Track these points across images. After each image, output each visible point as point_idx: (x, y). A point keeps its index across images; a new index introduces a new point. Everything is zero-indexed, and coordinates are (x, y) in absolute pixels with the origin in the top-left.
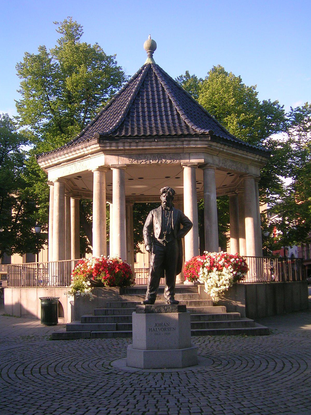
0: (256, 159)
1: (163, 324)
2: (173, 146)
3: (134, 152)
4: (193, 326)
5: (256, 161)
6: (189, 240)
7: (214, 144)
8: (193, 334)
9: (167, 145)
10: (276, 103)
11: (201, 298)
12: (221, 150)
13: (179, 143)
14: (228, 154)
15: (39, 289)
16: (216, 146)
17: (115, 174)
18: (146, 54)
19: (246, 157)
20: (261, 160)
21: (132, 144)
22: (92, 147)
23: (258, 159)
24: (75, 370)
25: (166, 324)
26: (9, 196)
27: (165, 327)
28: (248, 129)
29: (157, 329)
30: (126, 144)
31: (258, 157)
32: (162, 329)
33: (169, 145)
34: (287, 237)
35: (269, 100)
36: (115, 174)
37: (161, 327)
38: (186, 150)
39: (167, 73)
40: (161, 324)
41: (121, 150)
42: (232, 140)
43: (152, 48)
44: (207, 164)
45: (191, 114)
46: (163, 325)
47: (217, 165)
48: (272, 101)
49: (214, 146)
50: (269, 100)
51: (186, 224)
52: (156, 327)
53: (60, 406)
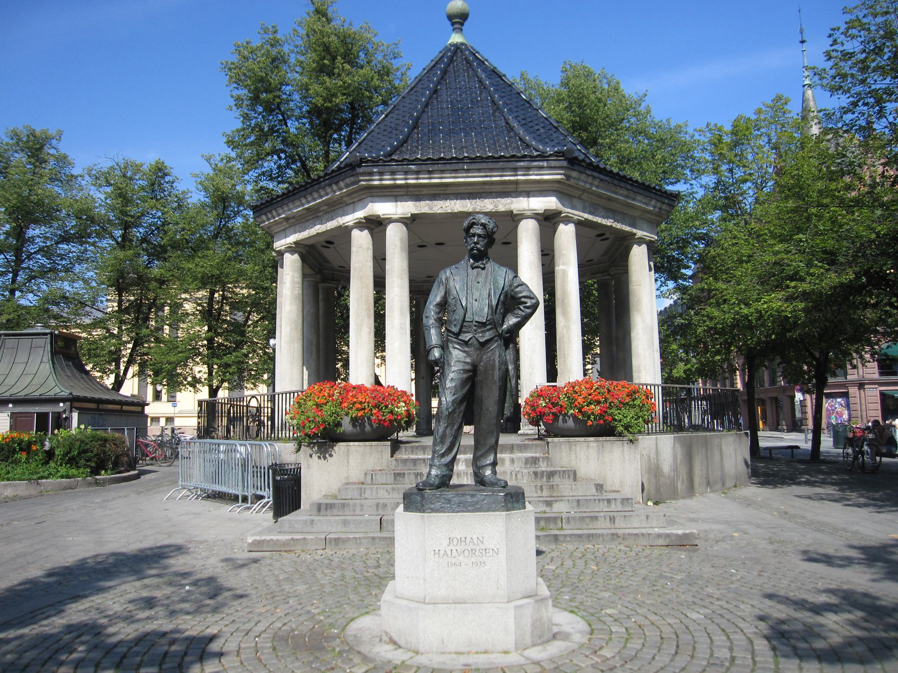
1: (468, 540)
3: (425, 191)
5: (648, 212)
6: (434, 421)
7: (574, 174)
10: (679, 129)
11: (551, 465)
12: (588, 186)
14: (599, 196)
15: (608, 445)
16: (579, 179)
20: (660, 209)
23: (654, 207)
25: (475, 540)
27: (474, 547)
29: (454, 551)
31: (653, 202)
32: (466, 553)
34: (771, 337)
35: (668, 120)
37: (464, 547)
38: (522, 186)
40: (463, 539)
46: (468, 542)
48: (673, 124)
49: (574, 178)
50: (668, 120)
51: (523, 300)
52: (452, 547)
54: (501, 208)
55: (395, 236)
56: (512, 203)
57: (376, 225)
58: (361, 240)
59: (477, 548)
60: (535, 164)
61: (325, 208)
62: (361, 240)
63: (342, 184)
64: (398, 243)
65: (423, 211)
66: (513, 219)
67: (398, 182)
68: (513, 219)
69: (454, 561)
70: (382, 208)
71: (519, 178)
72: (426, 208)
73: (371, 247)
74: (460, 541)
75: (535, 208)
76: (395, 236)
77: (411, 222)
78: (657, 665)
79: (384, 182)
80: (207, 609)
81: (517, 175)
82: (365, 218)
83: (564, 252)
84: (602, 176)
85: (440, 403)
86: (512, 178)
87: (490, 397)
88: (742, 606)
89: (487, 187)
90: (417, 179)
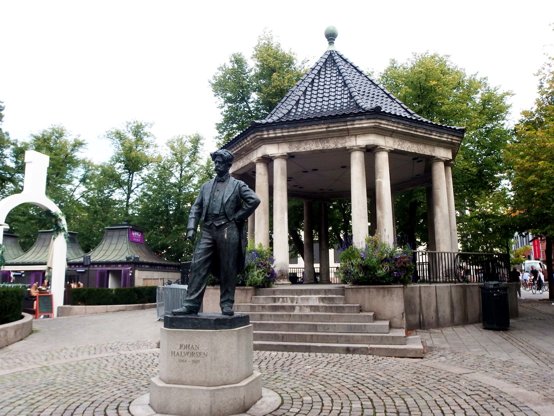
1: (191, 346)
25: (194, 346)
41: (279, 137)
43: (331, 37)
54: (340, 146)
55: (279, 166)
56: (346, 142)
57: (268, 161)
58: (260, 169)
59: (195, 352)
60: (357, 118)
61: (244, 152)
62: (260, 169)
63: (249, 139)
64: (279, 171)
65: (294, 151)
66: (347, 152)
67: (278, 135)
68: (347, 152)
69: (182, 358)
70: (271, 150)
71: (349, 127)
72: (296, 149)
73: (266, 173)
74: (186, 347)
75: (360, 144)
76: (279, 166)
77: (290, 157)
78: (335, 412)
79: (270, 136)
80: (493, 375)
81: (347, 125)
82: (262, 157)
83: (380, 170)
84: (404, 122)
85: (433, 256)
86: (344, 127)
87: (228, 262)
88: (309, 379)
89: (330, 134)
90: (289, 132)
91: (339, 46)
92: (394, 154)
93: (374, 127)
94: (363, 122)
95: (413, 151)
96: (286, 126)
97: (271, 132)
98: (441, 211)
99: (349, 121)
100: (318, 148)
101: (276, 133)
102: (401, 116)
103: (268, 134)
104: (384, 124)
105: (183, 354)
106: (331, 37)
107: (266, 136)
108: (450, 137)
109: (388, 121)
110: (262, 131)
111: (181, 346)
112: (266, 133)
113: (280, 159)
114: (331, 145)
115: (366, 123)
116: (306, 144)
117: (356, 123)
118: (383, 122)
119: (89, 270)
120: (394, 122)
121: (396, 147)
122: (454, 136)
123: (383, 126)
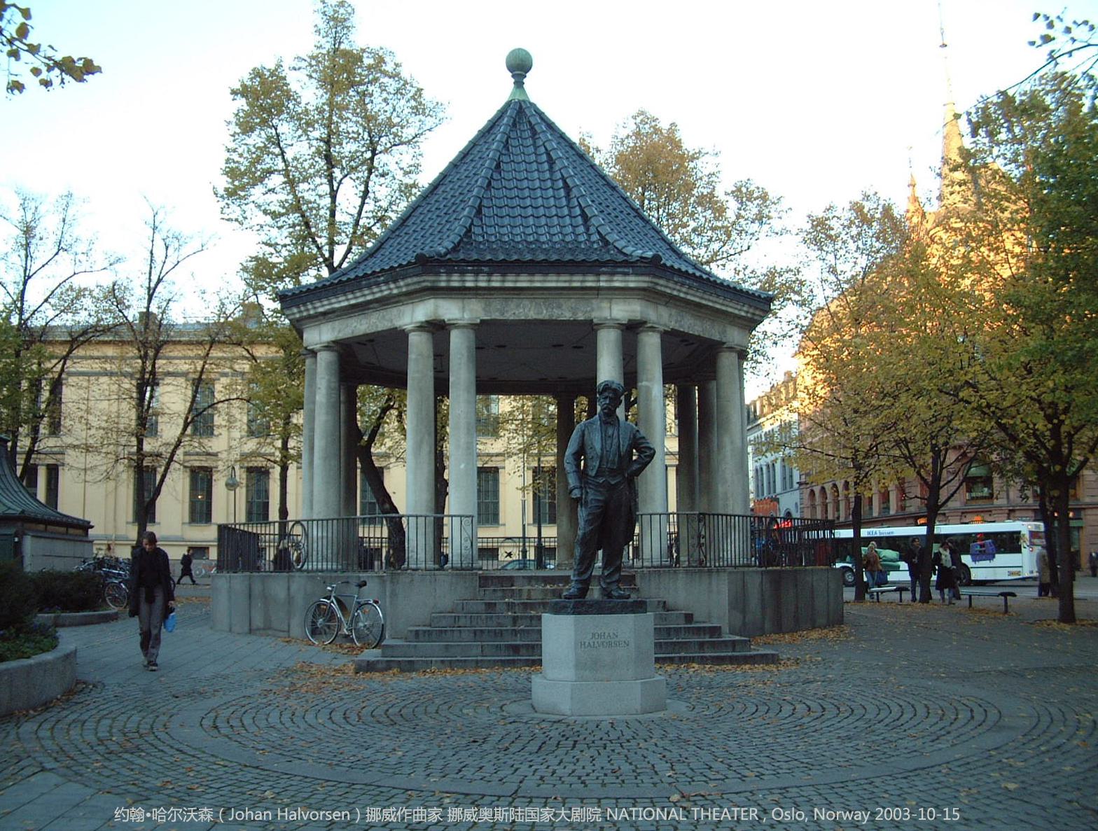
0: (743, 314)
2: (578, 284)
4: (658, 646)
8: (657, 660)
9: (565, 281)
13: (590, 278)
17: (459, 344)
18: (508, 80)
19: (724, 308)
21: (494, 278)
22: (409, 280)
24: (303, 725)
26: (1086, 114)
28: (1057, 142)
30: (481, 278)
33: (570, 281)
36: (459, 344)
39: (441, 173)
41: (469, 289)
42: (691, 271)
43: (520, 66)
44: (645, 322)
45: (609, 214)
47: (665, 325)
53: (917, 772)
56: (593, 310)
60: (619, 270)
68: (590, 329)
70: (449, 310)
91: (538, 91)
92: (671, 339)
93: (644, 289)
94: (627, 278)
95: (696, 333)
96: (486, 269)
97: (456, 277)
98: (732, 442)
99: (604, 273)
100: (540, 317)
101: (464, 281)
102: (680, 269)
103: (448, 281)
104: (665, 286)
105: (596, 645)
106: (520, 66)
107: (443, 284)
108: (751, 310)
109: (668, 280)
110: (438, 274)
111: (594, 635)
112: (444, 278)
113: (465, 330)
114: (565, 311)
115: (633, 282)
116: (518, 306)
117: (615, 278)
118: (662, 282)
119: (932, 537)
120: (676, 283)
121: (673, 325)
122: (757, 308)
123: (659, 288)
